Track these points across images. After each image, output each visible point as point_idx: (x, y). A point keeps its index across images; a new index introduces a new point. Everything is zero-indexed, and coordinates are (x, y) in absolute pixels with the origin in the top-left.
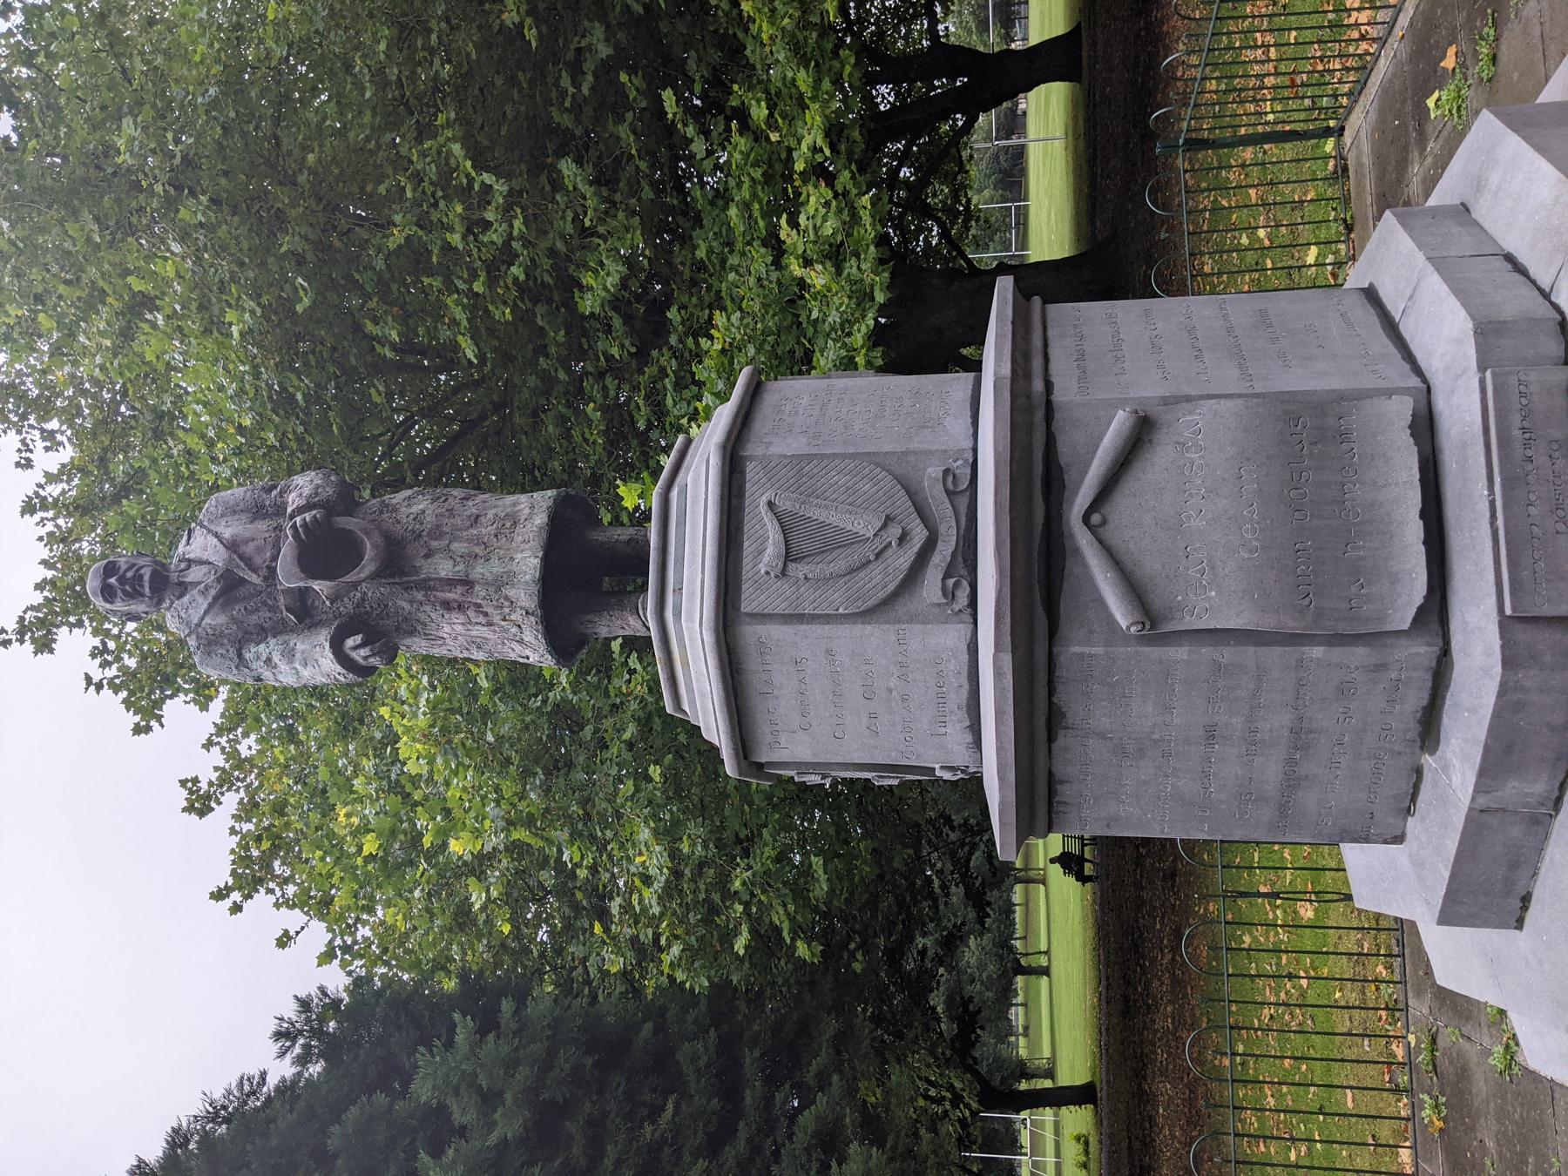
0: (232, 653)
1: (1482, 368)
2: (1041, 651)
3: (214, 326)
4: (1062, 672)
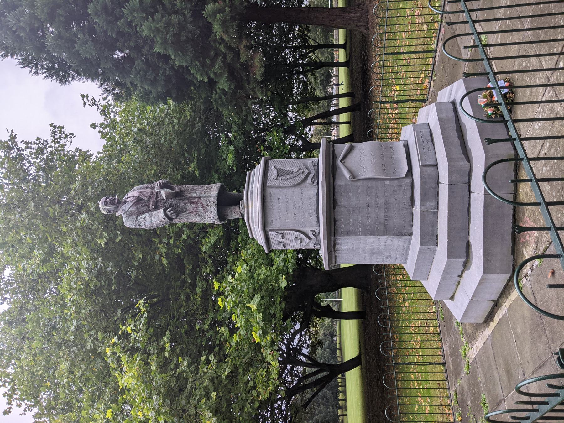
0: (135, 217)
1: (414, 131)
2: (332, 181)
4: (336, 190)
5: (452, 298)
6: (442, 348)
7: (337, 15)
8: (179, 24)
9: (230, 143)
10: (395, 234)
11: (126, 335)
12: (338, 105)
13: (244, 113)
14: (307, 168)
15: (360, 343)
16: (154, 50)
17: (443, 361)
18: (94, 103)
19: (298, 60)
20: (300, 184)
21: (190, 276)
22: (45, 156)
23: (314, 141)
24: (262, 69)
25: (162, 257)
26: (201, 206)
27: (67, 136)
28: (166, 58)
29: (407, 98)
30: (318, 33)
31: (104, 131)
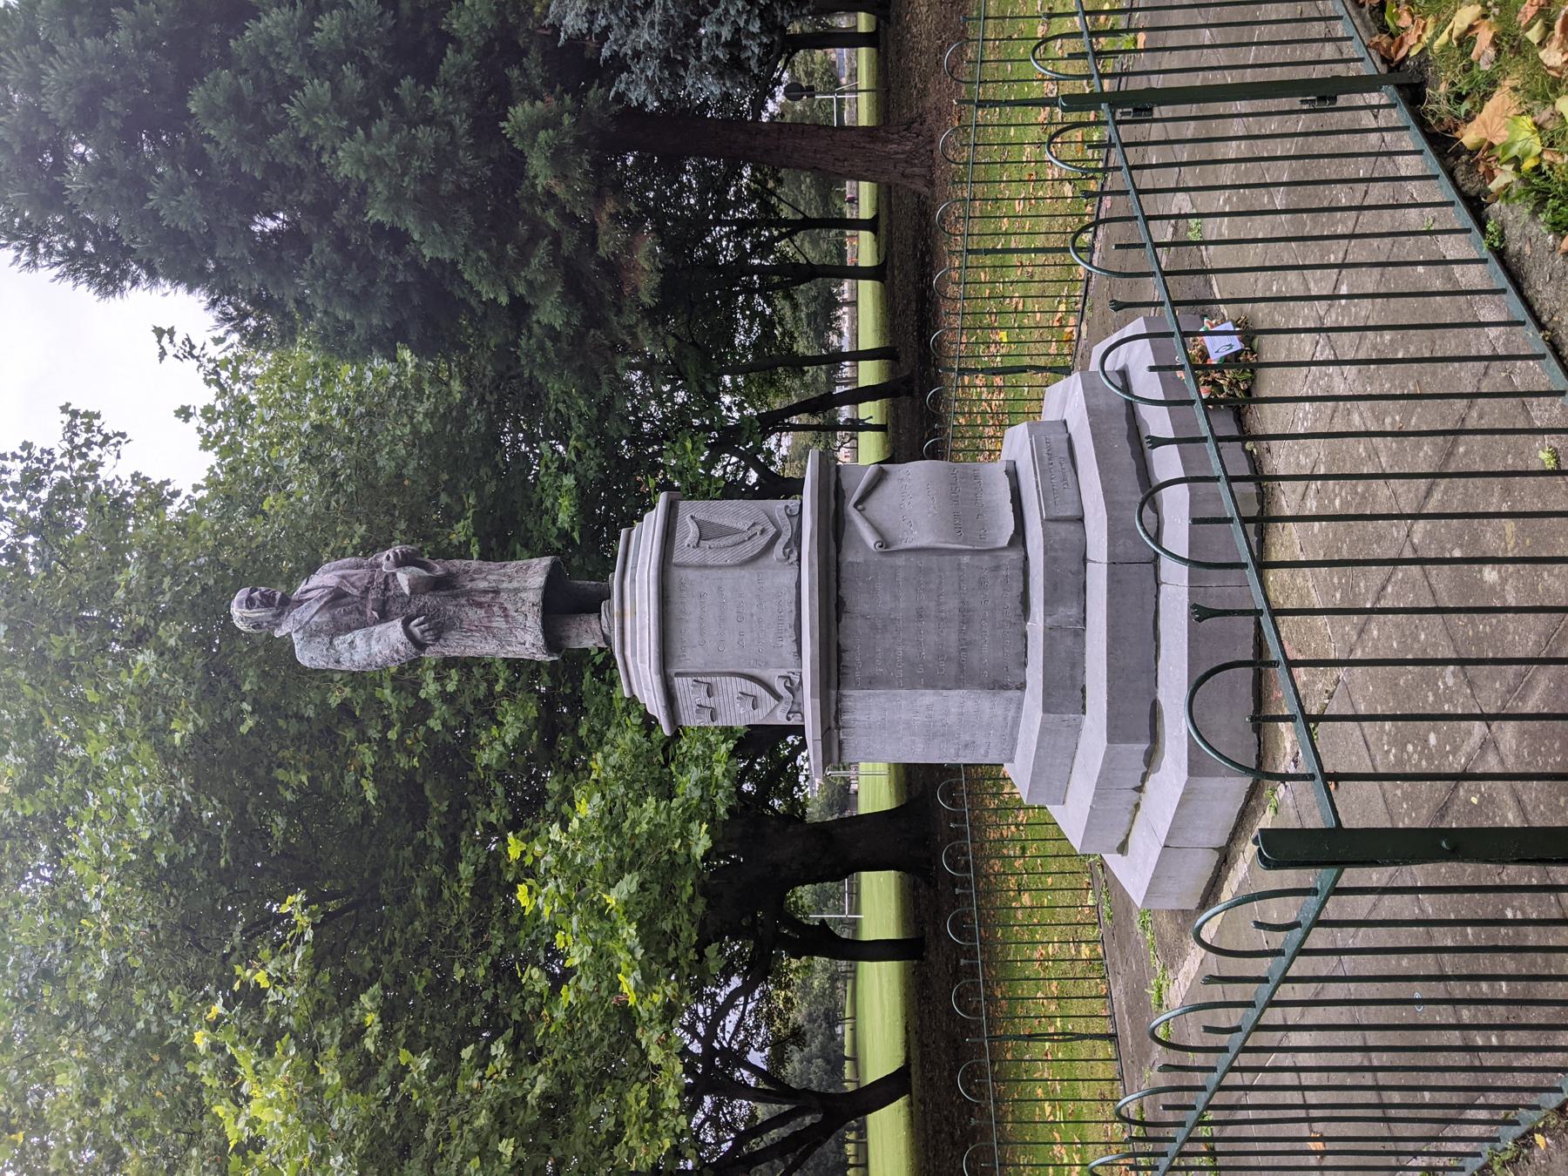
0: (327, 640)
3: (157, 734)
4: (843, 574)
5: (1123, 848)
6: (1108, 996)
7: (853, 147)
8: (436, 150)
9: (564, 468)
10: (982, 686)
11: (253, 997)
12: (855, 380)
13: (605, 390)
14: (774, 523)
15: (907, 1032)
16: (365, 215)
17: (1111, 1031)
18: (190, 351)
19: (750, 256)
20: (754, 559)
21: (442, 828)
22: (44, 494)
23: (788, 474)
24: (657, 278)
25: (364, 780)
26: (500, 613)
27: (107, 438)
28: (398, 239)
29: (1027, 361)
30: (803, 187)
31: (210, 429)
